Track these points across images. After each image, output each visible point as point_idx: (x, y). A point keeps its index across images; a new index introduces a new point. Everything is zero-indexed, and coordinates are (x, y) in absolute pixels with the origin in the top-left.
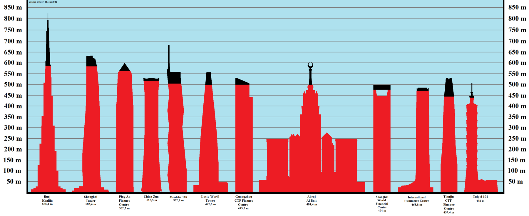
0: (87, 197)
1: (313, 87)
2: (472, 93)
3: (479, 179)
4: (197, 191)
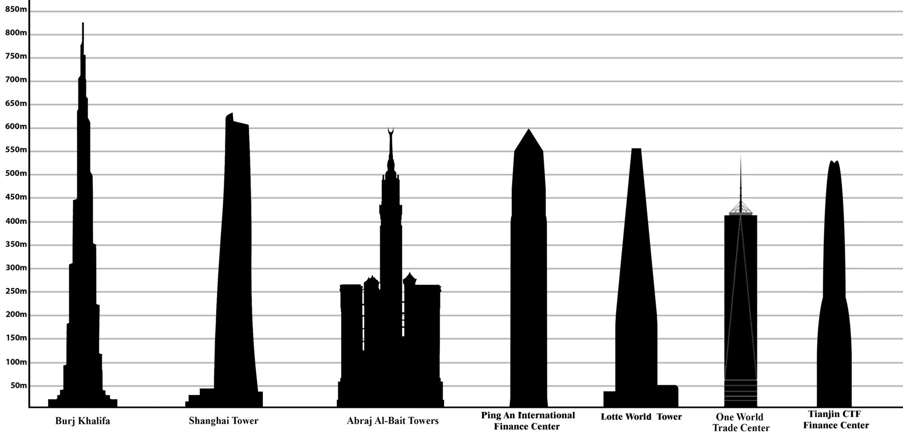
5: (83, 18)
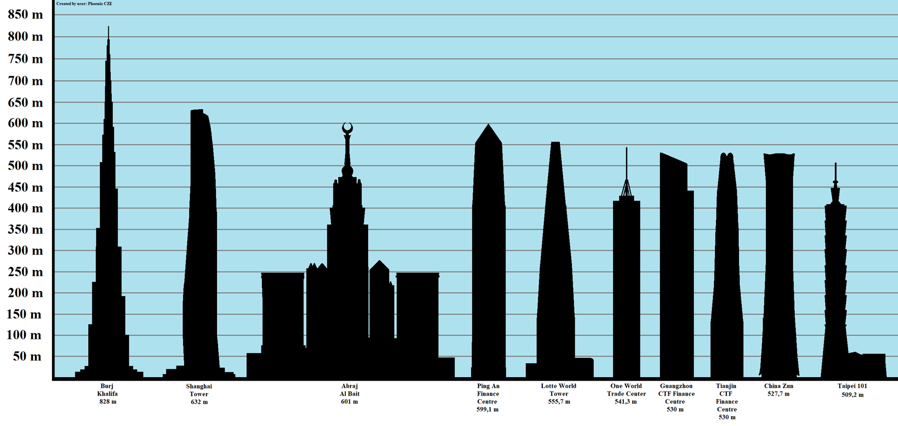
0: (191, 387)
1: (351, 171)
2: (836, 182)
3: (850, 351)
4: (533, 373)
5: (109, 21)
